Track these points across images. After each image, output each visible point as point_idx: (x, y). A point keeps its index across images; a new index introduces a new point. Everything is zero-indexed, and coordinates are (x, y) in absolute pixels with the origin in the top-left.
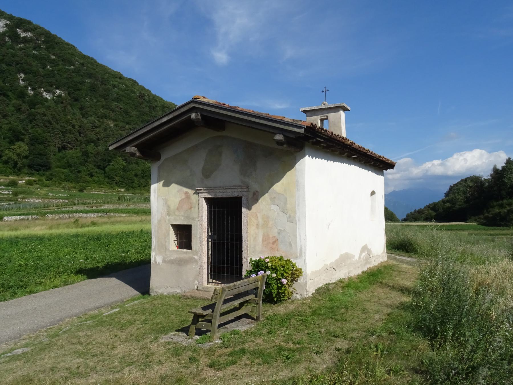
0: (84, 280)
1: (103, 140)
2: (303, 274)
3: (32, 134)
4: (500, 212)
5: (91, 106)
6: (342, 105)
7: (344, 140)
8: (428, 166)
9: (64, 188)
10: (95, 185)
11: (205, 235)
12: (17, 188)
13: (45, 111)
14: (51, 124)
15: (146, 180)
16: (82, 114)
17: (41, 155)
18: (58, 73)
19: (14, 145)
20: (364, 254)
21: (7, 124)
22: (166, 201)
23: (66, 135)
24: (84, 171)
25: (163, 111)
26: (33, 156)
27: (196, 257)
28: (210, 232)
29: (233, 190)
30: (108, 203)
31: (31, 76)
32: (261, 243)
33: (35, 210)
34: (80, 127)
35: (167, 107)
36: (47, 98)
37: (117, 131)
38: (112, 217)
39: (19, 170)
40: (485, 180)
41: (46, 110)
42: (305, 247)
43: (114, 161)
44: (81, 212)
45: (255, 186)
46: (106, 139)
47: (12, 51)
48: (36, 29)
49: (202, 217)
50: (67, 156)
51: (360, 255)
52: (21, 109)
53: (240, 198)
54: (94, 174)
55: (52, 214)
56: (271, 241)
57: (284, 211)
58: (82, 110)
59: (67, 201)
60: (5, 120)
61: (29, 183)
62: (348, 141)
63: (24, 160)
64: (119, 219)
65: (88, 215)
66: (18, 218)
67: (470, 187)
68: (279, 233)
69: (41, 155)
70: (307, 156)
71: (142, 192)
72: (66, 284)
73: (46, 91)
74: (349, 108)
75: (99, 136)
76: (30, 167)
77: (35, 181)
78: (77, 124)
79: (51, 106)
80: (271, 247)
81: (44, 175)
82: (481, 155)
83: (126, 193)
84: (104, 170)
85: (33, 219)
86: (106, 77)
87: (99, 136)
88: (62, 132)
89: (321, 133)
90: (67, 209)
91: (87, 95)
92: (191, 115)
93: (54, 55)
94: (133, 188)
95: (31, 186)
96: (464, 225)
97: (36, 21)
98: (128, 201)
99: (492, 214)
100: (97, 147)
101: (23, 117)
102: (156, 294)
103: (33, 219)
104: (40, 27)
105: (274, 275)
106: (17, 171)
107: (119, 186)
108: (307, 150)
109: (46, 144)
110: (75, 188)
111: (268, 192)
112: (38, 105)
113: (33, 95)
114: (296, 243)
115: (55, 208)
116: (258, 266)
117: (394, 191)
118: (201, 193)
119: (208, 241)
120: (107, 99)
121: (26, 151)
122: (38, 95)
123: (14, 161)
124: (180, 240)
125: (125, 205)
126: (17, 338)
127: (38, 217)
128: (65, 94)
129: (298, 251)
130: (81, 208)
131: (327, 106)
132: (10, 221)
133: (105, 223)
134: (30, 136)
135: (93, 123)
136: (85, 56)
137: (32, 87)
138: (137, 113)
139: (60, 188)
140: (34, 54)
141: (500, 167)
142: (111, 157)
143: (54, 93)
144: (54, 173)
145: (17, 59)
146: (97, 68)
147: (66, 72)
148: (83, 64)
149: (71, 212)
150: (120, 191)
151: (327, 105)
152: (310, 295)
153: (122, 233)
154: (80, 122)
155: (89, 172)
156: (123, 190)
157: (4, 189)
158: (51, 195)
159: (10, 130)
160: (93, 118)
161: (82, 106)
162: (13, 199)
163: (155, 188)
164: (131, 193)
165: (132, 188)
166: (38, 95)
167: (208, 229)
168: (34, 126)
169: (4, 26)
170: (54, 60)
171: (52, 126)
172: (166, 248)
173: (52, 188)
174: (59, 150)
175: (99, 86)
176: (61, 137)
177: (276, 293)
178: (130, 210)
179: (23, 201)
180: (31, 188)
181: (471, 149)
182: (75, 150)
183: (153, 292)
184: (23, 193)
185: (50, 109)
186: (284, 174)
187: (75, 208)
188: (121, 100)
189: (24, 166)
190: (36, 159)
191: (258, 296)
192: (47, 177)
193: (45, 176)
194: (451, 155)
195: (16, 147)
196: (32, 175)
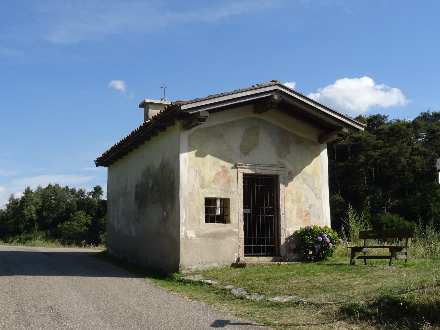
45: (290, 168)
56: (304, 214)
68: (310, 207)
80: (304, 219)
111: (300, 172)
118: (241, 168)
129: (325, 221)
186: (312, 159)
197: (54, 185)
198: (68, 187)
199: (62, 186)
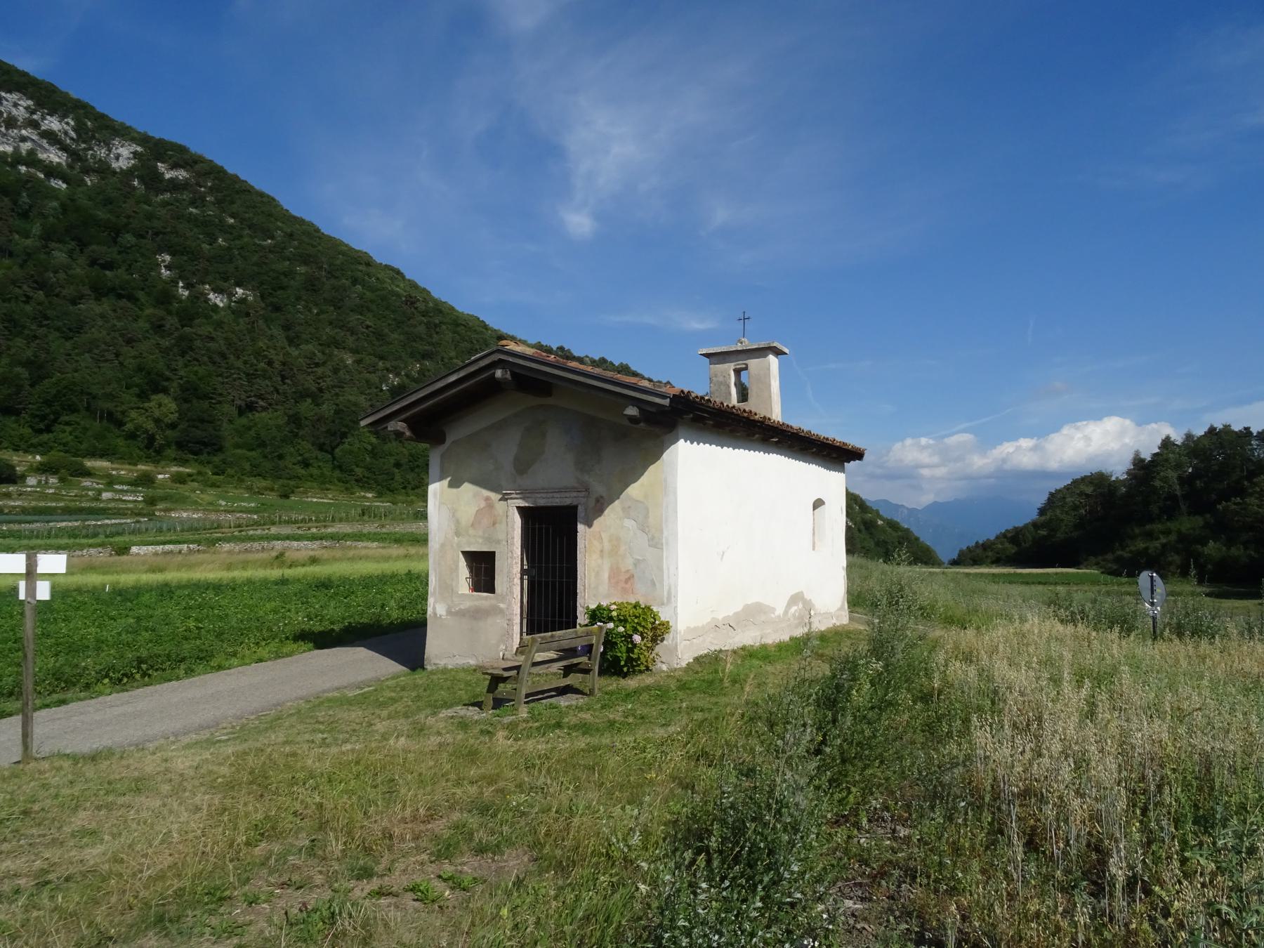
0: (310, 650)
1: (330, 392)
2: (671, 629)
3: (185, 379)
4: (1147, 548)
5: (306, 322)
6: (772, 345)
7: (746, 415)
8: (1006, 451)
9: (249, 489)
10: (315, 484)
11: (517, 569)
12: (155, 488)
13: (211, 330)
14: (226, 359)
15: (419, 476)
16: (288, 338)
17: (202, 421)
18: (239, 254)
19: (149, 400)
20: (794, 609)
21: (135, 357)
22: (454, 512)
23: (254, 381)
24: (291, 454)
25: (455, 332)
26: (187, 424)
27: (502, 606)
28: (525, 563)
29: (563, 495)
30: (341, 520)
31: (185, 258)
32: (607, 581)
33: (194, 534)
34: (284, 364)
35: (464, 325)
36: (215, 305)
37: (360, 373)
38: (350, 548)
39: (159, 452)
40: (1117, 480)
41: (215, 330)
42: (676, 587)
43: (353, 435)
44: (288, 538)
45: (599, 489)
46: (337, 390)
47: (146, 207)
48: (196, 162)
49: (513, 538)
50: (256, 424)
51: (786, 607)
52: (162, 326)
53: (575, 508)
54: (311, 461)
55: (228, 543)
56: (623, 577)
57: (643, 528)
58: (289, 329)
59: (255, 517)
60: (130, 349)
61: (179, 479)
62: (756, 414)
63: (167, 432)
64: (364, 552)
65: (302, 544)
66: (159, 548)
67: (1087, 496)
68: (635, 565)
69: (202, 421)
70: (682, 441)
71: (409, 499)
72: (278, 656)
73: (215, 290)
74: (786, 350)
75: (322, 384)
76: (180, 445)
77: (190, 475)
78: (277, 358)
79: (226, 320)
80: (623, 588)
81: (208, 463)
82: (1122, 433)
83: (377, 502)
84: (332, 454)
85: (190, 550)
86: (338, 262)
87: (322, 384)
88: (248, 375)
89: (702, 404)
90: (259, 532)
91: (298, 298)
92: (494, 373)
93: (232, 216)
94: (392, 491)
95: (182, 486)
96: (1073, 573)
97: (197, 146)
98: (381, 517)
99: (1131, 552)
100: (318, 405)
101: (167, 343)
102: (434, 668)
103: (190, 550)
104: (203, 158)
105: (621, 629)
106: (153, 454)
107: (362, 488)
108: (681, 430)
109: (215, 399)
110: (272, 490)
111: (618, 498)
112: (198, 319)
113: (188, 297)
114: (662, 581)
115: (232, 530)
116: (596, 615)
117: (935, 503)
118: (511, 498)
119: (522, 579)
120: (339, 308)
121: (172, 413)
122: (197, 298)
123: (148, 434)
124: (476, 576)
125: (376, 525)
126: (212, 727)
127: (201, 548)
128: (255, 296)
129: (665, 593)
130: (286, 530)
131: (746, 346)
132: (145, 554)
133: (335, 559)
134: (182, 382)
135: (311, 357)
136: (295, 218)
137: (187, 281)
138: (402, 337)
139: (242, 491)
140: (191, 213)
141: (1147, 455)
142: (347, 426)
143: (231, 295)
144: (229, 459)
145: (156, 224)
146: (319, 244)
147: (256, 252)
148: (291, 235)
149: (267, 538)
150: (364, 497)
151: (747, 344)
152: (684, 664)
153: (371, 577)
154: (284, 355)
155: (299, 458)
156: (370, 495)
157: (127, 491)
158: (224, 503)
159: (140, 369)
160: (310, 347)
161: (288, 321)
162: (145, 512)
163: (436, 490)
164: (388, 502)
165: (390, 491)
166: (197, 298)
167: (522, 554)
168: (189, 361)
169: (131, 156)
170: (232, 226)
171: (227, 363)
172: (452, 590)
173: (225, 489)
174: (241, 412)
175: (325, 280)
176: (244, 385)
177: (625, 658)
178: (386, 536)
179: (166, 516)
180: (184, 490)
181: (1097, 416)
182: (273, 413)
183: (430, 665)
184: (164, 498)
185: (222, 328)
186: (645, 468)
187: (274, 530)
188: (369, 310)
189: (168, 445)
190: (194, 429)
191: (593, 658)
192: (216, 467)
193: (210, 465)
194: (1057, 429)
195: (152, 404)
196: (184, 462)
197: (1221, 427)
198: (1249, 428)
199: (1237, 427)
